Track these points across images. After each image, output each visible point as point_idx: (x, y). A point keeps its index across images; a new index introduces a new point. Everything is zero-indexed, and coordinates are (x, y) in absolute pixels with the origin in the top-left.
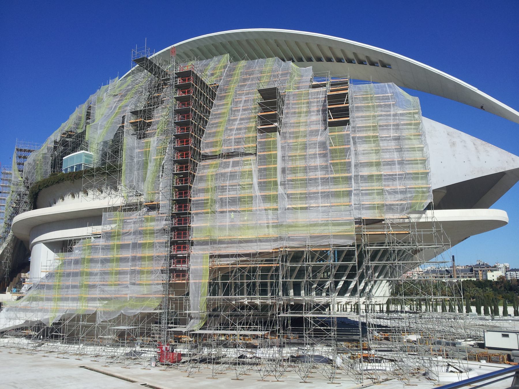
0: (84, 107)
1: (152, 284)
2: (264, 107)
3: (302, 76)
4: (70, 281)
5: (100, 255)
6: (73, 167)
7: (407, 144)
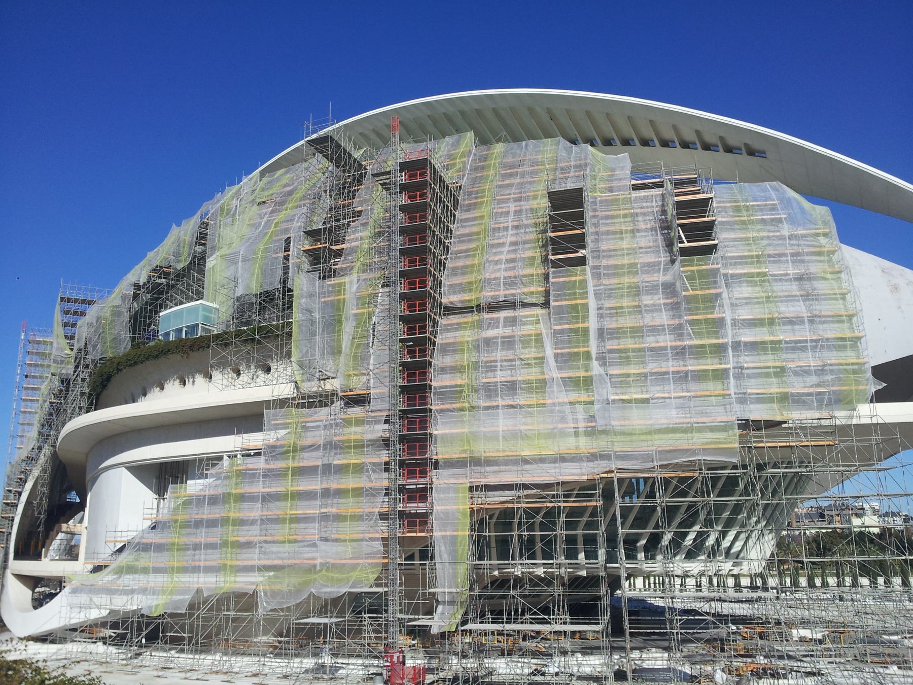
1: (362, 540)
2: (556, 223)
3: (613, 170)
4: (202, 536)
5: (259, 488)
6: (180, 330)
7: (821, 287)
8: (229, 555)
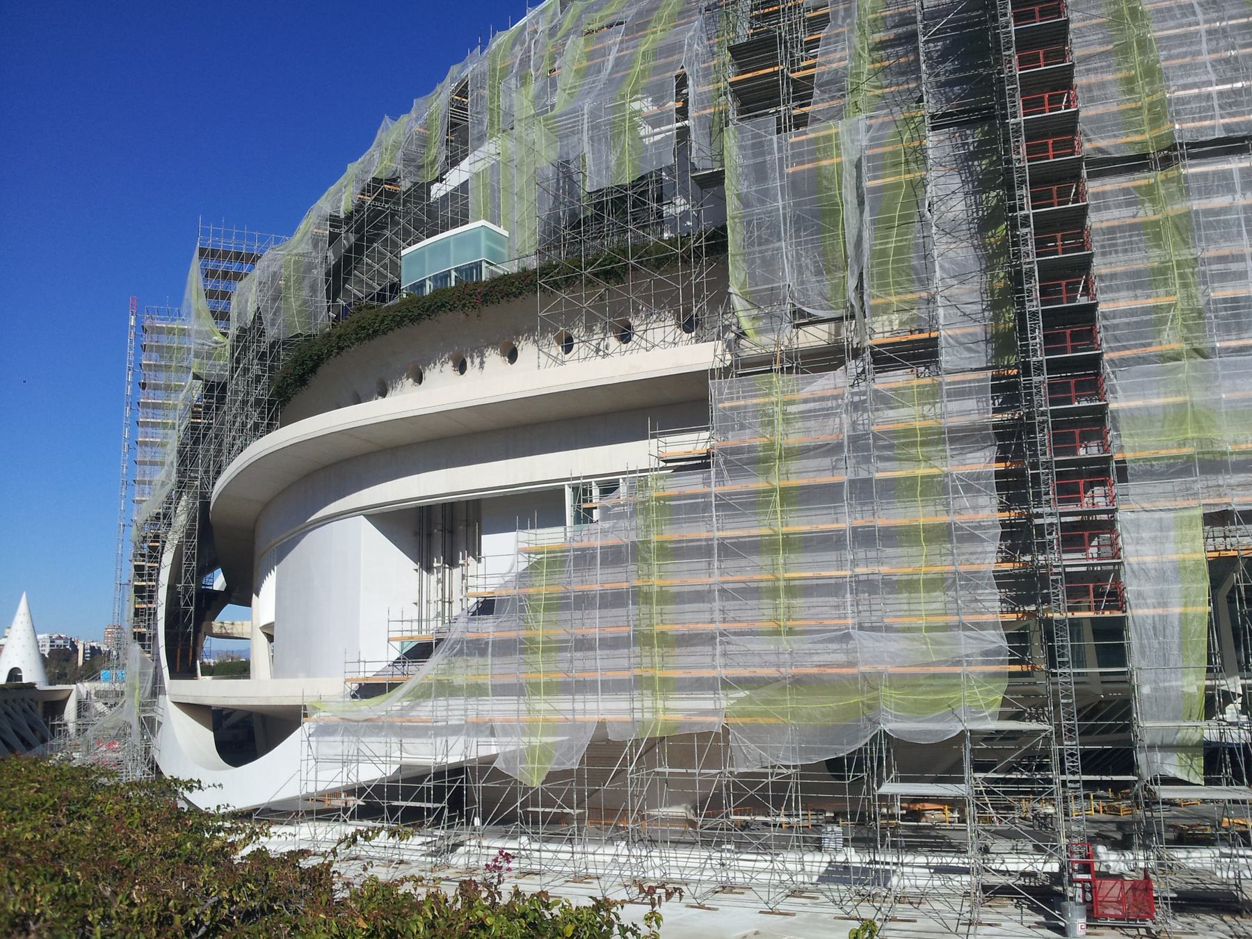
0: (439, 101)
4: (595, 625)
6: (421, 285)
8: (657, 659)
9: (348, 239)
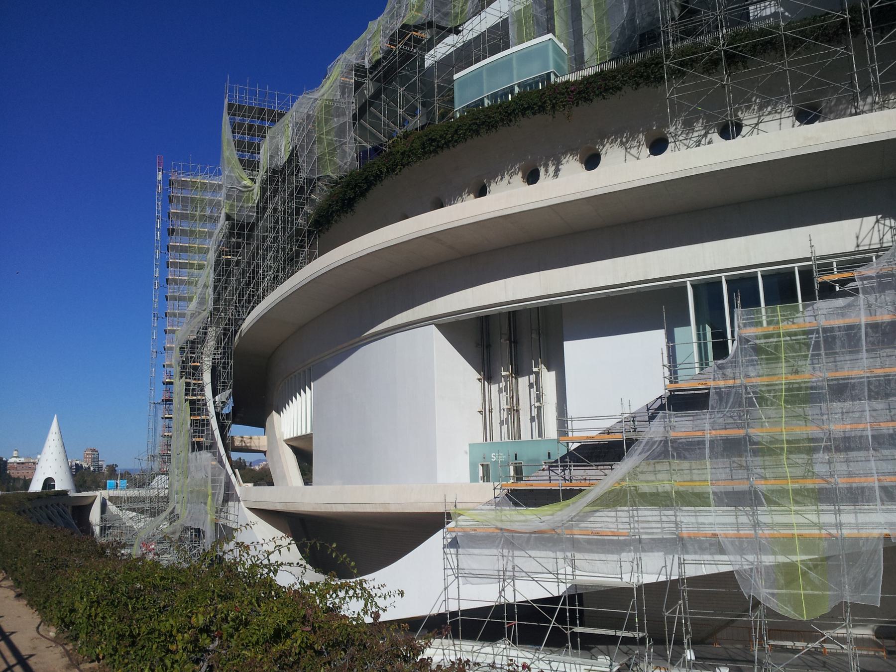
9: (369, 88)
